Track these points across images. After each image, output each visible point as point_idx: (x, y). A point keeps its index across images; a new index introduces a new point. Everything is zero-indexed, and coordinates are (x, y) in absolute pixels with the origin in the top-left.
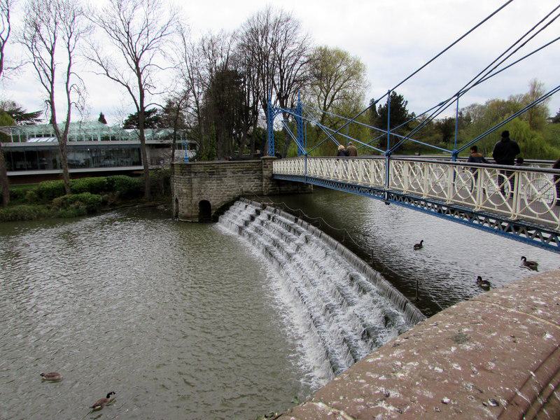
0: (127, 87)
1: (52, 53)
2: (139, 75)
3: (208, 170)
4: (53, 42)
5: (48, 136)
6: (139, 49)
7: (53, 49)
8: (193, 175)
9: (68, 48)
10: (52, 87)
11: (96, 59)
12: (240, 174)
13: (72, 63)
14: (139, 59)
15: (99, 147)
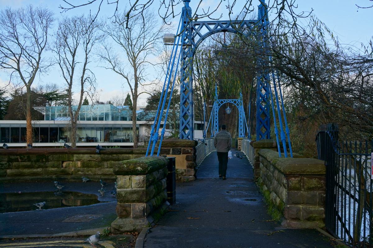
0: (127, 79)
4: (75, 47)
5: (124, 119)
6: (136, 50)
9: (86, 51)
10: (71, 80)
11: (107, 57)
13: (88, 62)
14: (136, 58)
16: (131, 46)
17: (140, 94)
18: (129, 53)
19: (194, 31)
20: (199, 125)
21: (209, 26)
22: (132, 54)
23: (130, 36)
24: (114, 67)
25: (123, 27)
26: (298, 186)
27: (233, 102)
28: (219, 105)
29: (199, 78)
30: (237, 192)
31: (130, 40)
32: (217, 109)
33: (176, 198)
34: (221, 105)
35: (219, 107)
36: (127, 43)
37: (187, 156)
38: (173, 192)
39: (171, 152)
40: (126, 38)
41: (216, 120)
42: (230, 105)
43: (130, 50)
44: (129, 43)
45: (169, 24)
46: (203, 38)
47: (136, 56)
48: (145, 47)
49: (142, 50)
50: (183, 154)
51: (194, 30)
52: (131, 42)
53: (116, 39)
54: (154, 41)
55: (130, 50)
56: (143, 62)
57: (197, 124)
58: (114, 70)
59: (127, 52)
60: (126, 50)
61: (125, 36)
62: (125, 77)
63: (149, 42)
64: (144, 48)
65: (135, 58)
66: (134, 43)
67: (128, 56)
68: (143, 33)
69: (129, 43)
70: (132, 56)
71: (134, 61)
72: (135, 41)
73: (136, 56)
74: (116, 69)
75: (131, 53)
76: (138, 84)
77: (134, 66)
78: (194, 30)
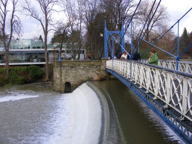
0: (40, 21)
1: (5, 6)
2: (46, 15)
3: (71, 65)
7: (6, 4)
8: (62, 68)
10: (4, 22)
12: (88, 68)
13: (15, 10)
14: (47, 7)
15: (22, 52)
22: (44, 5)
24: (32, 14)
47: (46, 6)
49: (50, 2)
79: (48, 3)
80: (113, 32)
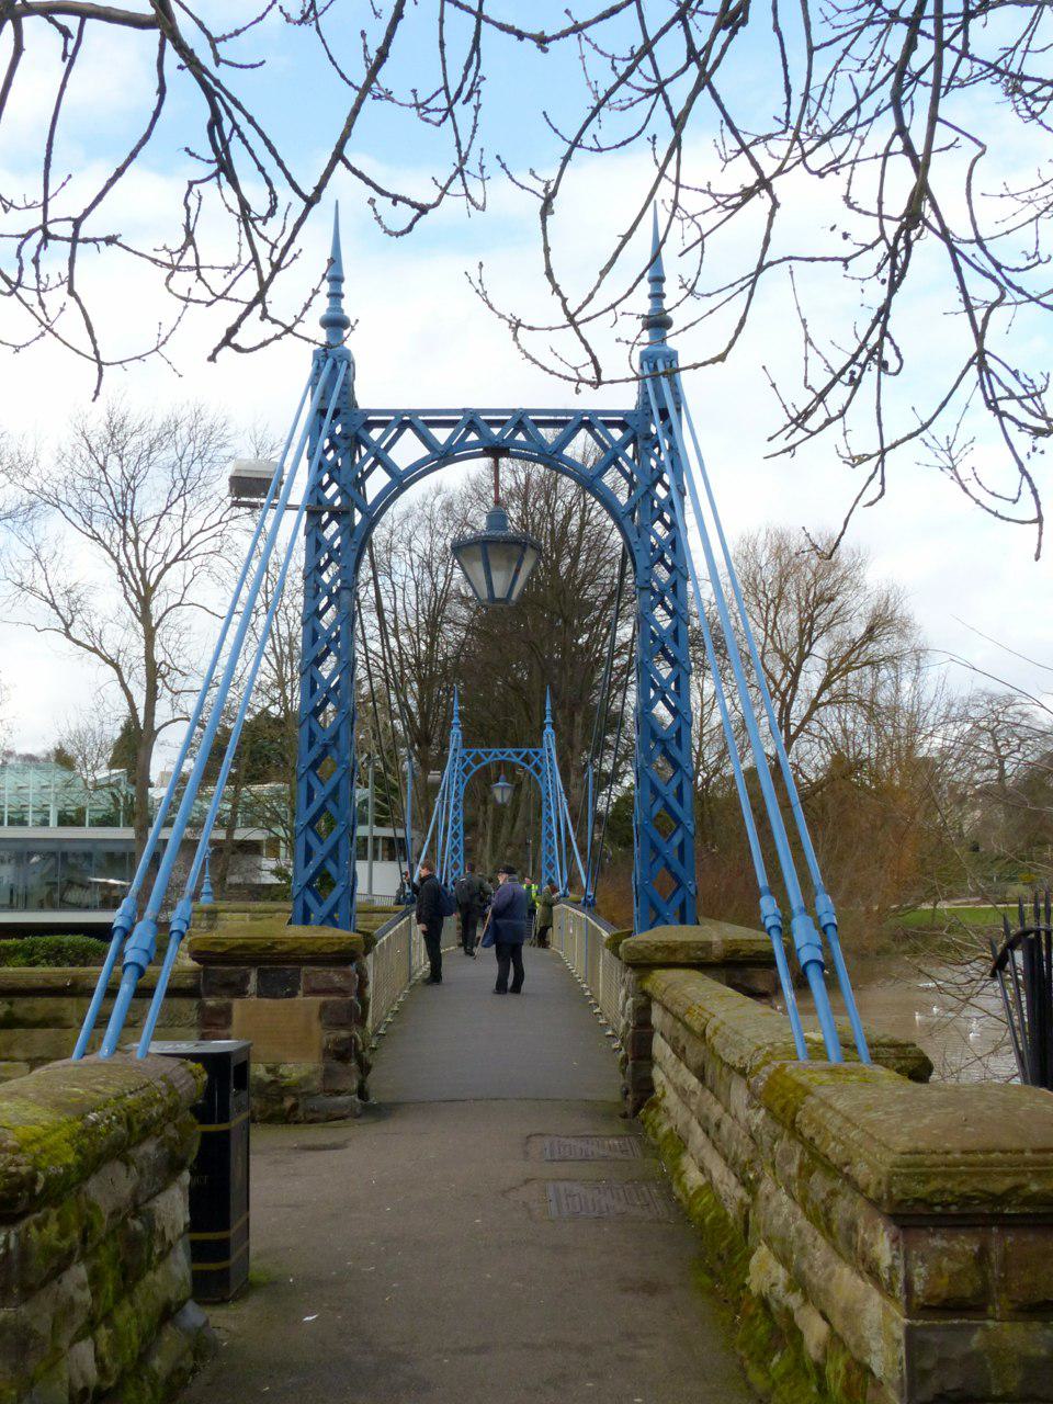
6: (153, 560)
14: (154, 589)
16: (136, 544)
17: (166, 724)
18: (127, 571)
19: (364, 451)
20: (390, 841)
21: (431, 430)
22: (138, 576)
23: (129, 508)
24: (68, 626)
25: (102, 473)
26: (967, 1290)
27: (517, 760)
28: (466, 771)
29: (385, 664)
30: (557, 1190)
31: (129, 523)
32: (460, 784)
33: (253, 1264)
34: (476, 768)
35: (467, 778)
36: (118, 536)
37: (324, 1006)
38: (235, 1227)
39: (252, 986)
40: (115, 514)
41: (455, 842)
42: (505, 768)
43: (129, 561)
44: (126, 534)
45: (171, 282)
46: (401, 481)
47: (152, 584)
48: (186, 550)
49: (175, 560)
50: (307, 993)
51: (362, 448)
52: (136, 529)
53: (79, 522)
54: (221, 527)
55: (129, 561)
56: (180, 604)
57: (384, 838)
58: (68, 635)
59: (120, 567)
60: (116, 559)
61: (112, 507)
62: (107, 662)
63: (201, 531)
64: (183, 553)
65: (150, 590)
66: (145, 536)
67: (122, 582)
68: (179, 496)
69: (126, 534)
70: (136, 582)
71: (145, 601)
72: (152, 525)
73: (152, 584)
74: (75, 631)
75: (132, 573)
76: (157, 687)
77: (145, 617)
78: (362, 448)
79: (162, 566)
80: (496, 756)
